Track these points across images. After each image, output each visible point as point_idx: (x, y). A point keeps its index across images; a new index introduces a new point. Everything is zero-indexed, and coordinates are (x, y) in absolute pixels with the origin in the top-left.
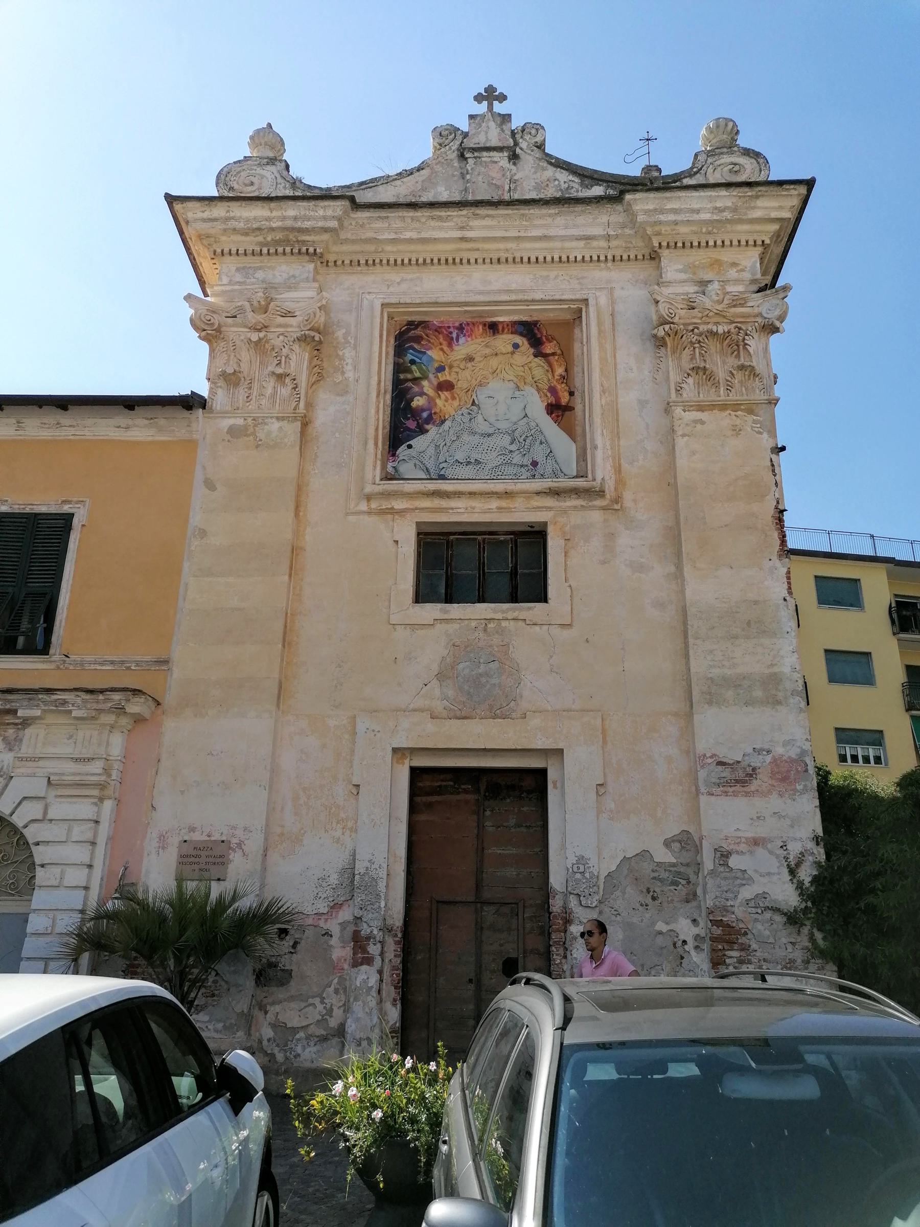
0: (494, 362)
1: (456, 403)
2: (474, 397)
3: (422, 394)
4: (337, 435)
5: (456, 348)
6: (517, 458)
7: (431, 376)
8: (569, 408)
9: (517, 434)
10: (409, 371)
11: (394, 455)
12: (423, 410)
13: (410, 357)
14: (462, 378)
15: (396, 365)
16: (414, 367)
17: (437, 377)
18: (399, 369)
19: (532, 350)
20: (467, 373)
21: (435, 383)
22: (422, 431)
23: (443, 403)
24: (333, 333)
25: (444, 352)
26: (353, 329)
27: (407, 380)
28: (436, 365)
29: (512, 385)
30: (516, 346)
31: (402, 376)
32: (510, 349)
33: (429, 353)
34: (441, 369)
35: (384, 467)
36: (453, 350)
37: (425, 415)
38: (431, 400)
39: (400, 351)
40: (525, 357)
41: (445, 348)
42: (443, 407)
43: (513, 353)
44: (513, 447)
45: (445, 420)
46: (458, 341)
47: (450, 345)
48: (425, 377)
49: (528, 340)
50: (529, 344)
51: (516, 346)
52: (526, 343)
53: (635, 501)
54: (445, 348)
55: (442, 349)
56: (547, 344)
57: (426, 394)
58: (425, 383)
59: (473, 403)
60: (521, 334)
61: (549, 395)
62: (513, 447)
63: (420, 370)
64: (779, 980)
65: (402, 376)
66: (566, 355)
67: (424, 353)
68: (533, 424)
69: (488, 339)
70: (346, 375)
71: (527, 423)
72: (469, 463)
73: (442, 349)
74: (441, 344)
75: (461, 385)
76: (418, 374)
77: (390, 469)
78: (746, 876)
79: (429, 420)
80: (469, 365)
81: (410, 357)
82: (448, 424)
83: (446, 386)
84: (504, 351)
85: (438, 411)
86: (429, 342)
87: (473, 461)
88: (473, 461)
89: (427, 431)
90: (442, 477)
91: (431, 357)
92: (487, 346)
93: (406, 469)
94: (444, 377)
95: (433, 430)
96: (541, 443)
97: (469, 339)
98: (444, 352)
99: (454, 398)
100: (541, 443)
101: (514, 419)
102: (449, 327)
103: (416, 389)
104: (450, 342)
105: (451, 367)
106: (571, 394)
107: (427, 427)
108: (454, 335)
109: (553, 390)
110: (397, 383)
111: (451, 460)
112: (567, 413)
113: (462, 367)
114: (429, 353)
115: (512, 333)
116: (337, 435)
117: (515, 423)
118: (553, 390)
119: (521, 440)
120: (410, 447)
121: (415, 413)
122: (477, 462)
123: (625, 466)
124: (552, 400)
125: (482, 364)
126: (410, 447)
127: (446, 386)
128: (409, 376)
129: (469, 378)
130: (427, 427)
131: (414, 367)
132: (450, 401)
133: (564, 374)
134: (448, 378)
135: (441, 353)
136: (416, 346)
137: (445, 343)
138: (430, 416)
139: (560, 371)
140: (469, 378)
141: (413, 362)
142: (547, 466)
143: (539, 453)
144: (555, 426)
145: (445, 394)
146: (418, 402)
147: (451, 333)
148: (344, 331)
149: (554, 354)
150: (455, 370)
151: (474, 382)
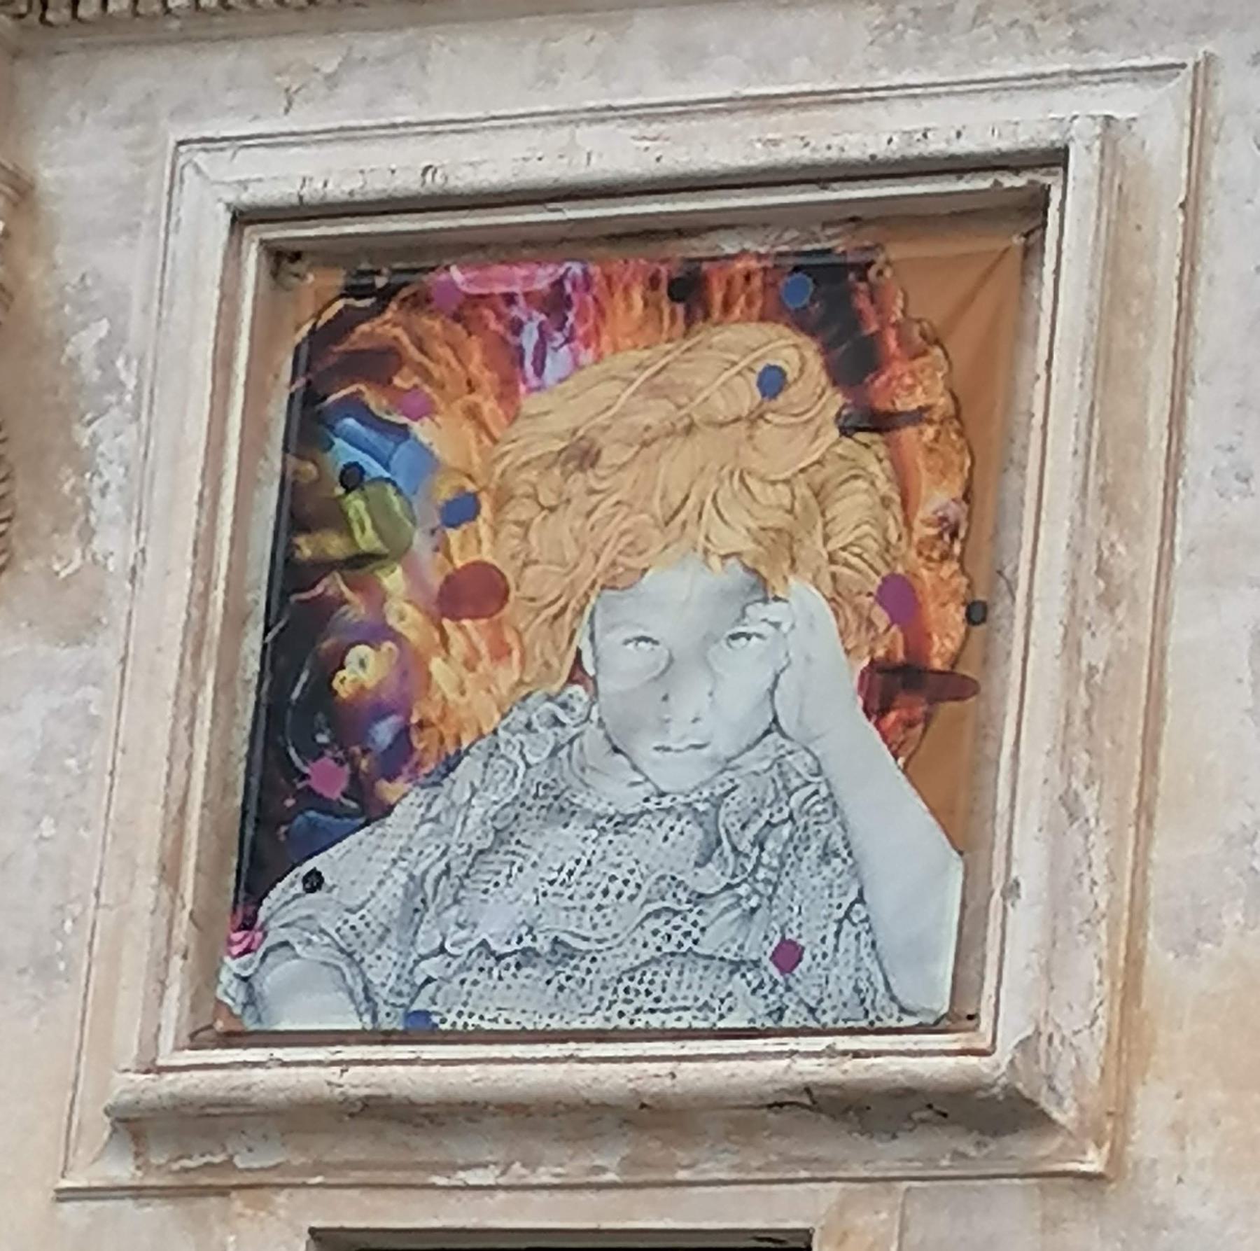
0: (676, 467)
1: (507, 675)
2: (582, 641)
3: (377, 633)
4: (47, 827)
5: (530, 404)
6: (721, 931)
7: (420, 542)
8: (956, 686)
9: (728, 818)
10: (341, 523)
11: (248, 924)
12: (380, 712)
13: (344, 452)
14: (535, 548)
15: (290, 489)
16: (356, 504)
17: (443, 548)
18: (299, 513)
19: (835, 401)
20: (566, 524)
21: (436, 581)
22: (372, 810)
23: (460, 679)
24: (62, 339)
25: (482, 426)
26: (136, 324)
27: (324, 566)
28: (445, 493)
29: (735, 574)
30: (772, 382)
31: (306, 549)
32: (748, 396)
33: (422, 430)
34: (461, 511)
35: (208, 974)
36: (513, 419)
37: (384, 733)
38: (412, 668)
39: (310, 423)
40: (804, 436)
41: (489, 407)
42: (453, 696)
43: (756, 417)
44: (709, 879)
45: (459, 756)
46: (539, 370)
47: (507, 392)
48: (397, 552)
49: (826, 349)
50: (829, 367)
51: (772, 382)
52: (815, 364)
53: (1178, 1129)
54: (489, 407)
55: (473, 413)
56: (898, 368)
57: (396, 637)
58: (393, 580)
59: (577, 674)
60: (801, 323)
61: (881, 618)
62: (709, 879)
63: (380, 512)
64: (180, 925)
65: (306, 549)
66: (980, 428)
67: (403, 432)
68: (800, 763)
69: (663, 353)
70: (96, 544)
71: (778, 762)
72: (528, 956)
73: (473, 413)
74: (471, 386)
75: (533, 584)
76: (368, 540)
77: (229, 990)
78: (1062, 16)
79: (398, 759)
80: (577, 484)
81: (344, 452)
82: (468, 770)
83: (473, 594)
84: (722, 407)
85: (434, 715)
86: (427, 376)
87: (543, 945)
88: (543, 945)
89: (388, 810)
90: (420, 1029)
91: (425, 450)
92: (653, 390)
93: (304, 996)
94: (477, 545)
95: (408, 803)
96: (826, 855)
97: (587, 356)
98: (482, 426)
99: (501, 652)
100: (826, 855)
101: (723, 746)
102: (510, 299)
103: (356, 609)
104: (512, 371)
105: (503, 499)
106: (976, 614)
107: (389, 790)
108: (529, 339)
109: (899, 596)
110: (290, 575)
111: (412, 830)
112: (947, 708)
113: (548, 498)
114: (422, 430)
115: (762, 319)
116: (47, 827)
117: (727, 764)
118: (899, 596)
119: (744, 846)
120: (314, 882)
121: (349, 722)
122: (561, 951)
123: (1160, 958)
124: (890, 642)
125: (627, 477)
126: (314, 882)
127: (473, 594)
128: (335, 546)
129: (571, 553)
130: (389, 790)
131: (356, 504)
132: (484, 665)
133: (956, 512)
134: (486, 555)
135: (468, 429)
136: (374, 400)
137: (487, 378)
138: (403, 734)
139: (938, 497)
140: (571, 553)
141: (352, 478)
142: (830, 977)
143: (808, 909)
144: (890, 766)
145: (467, 634)
146: (363, 670)
147: (517, 327)
148: (103, 328)
149: (920, 416)
150: (521, 510)
151: (588, 570)
